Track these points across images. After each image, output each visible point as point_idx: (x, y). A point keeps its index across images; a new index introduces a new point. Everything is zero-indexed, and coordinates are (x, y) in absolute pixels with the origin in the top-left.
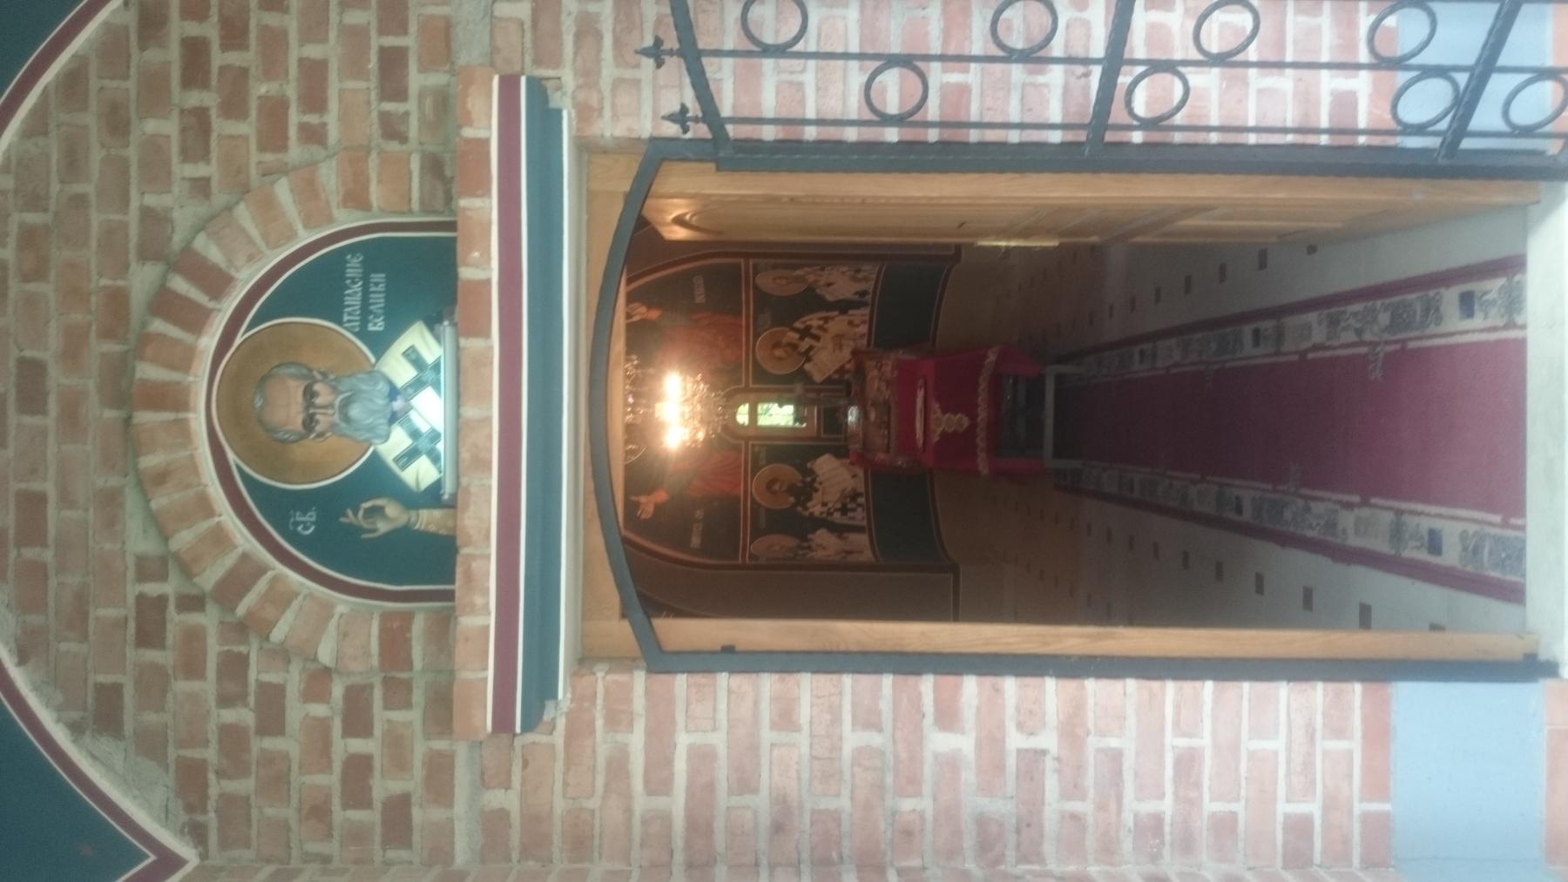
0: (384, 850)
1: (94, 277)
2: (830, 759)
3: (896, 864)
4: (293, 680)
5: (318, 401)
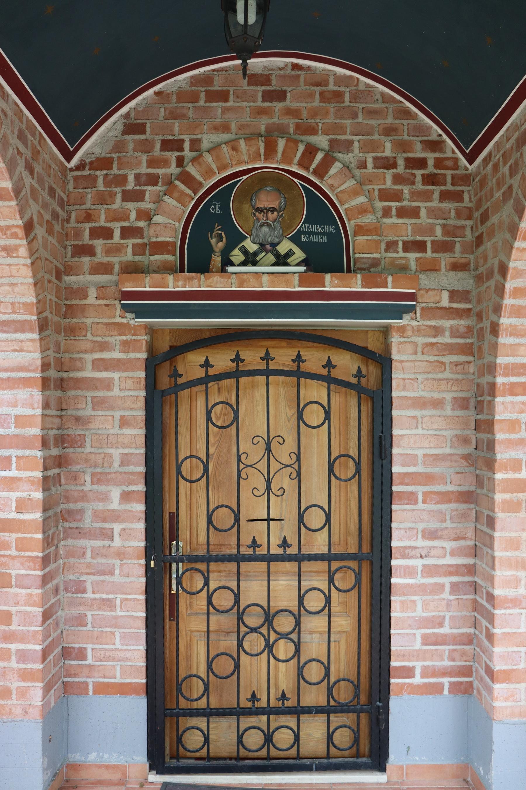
0: (71, 246)
1: (322, 121)
2: (107, 443)
3: (62, 473)
4: (146, 205)
5: (270, 214)
